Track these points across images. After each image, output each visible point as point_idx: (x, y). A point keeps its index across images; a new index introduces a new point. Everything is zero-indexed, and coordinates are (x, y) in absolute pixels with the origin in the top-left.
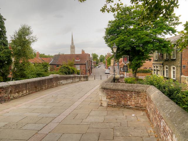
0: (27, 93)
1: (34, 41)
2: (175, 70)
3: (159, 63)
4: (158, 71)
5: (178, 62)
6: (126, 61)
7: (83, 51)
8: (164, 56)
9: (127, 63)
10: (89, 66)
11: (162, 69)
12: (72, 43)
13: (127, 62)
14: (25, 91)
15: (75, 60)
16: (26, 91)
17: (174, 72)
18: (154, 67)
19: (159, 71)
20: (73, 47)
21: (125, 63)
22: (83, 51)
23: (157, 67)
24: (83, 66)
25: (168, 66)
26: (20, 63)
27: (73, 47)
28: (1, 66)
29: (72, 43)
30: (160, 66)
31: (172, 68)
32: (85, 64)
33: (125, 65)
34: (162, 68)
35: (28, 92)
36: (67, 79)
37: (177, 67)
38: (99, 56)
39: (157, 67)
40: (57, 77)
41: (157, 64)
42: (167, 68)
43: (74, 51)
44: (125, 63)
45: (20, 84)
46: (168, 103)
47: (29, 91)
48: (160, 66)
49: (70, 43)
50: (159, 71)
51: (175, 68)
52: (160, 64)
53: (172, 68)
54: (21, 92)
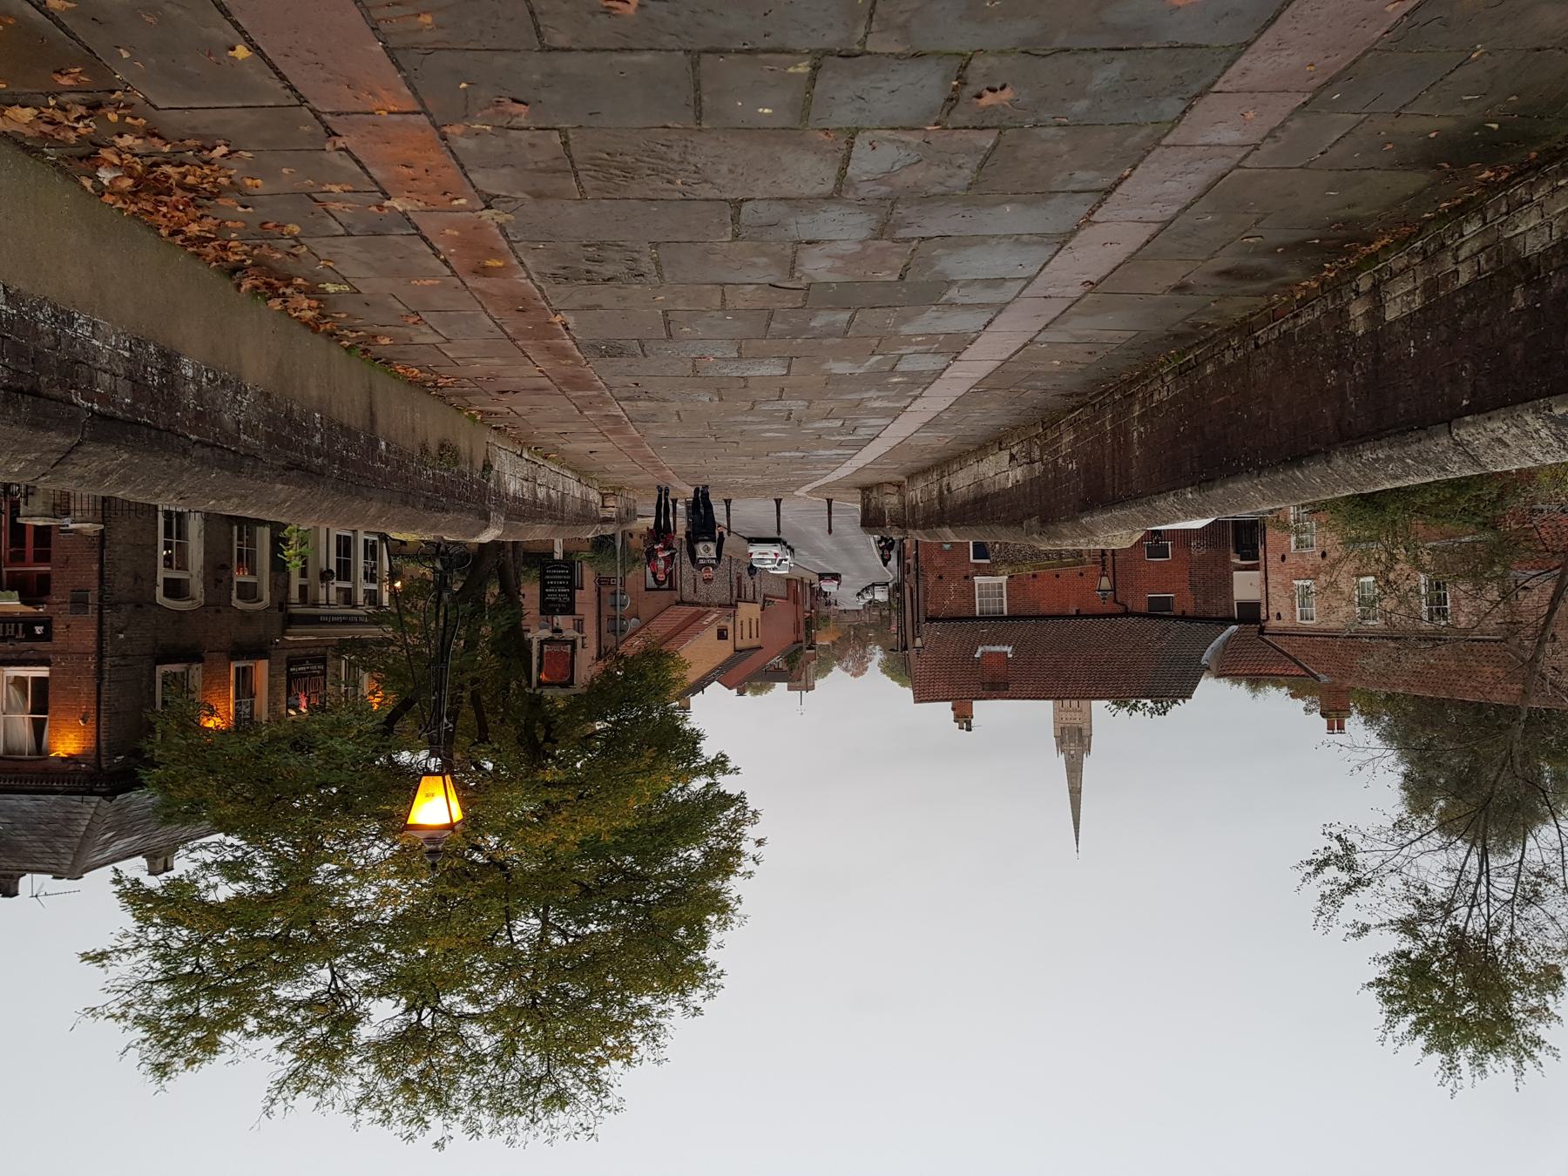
0: (1365, 283)
1: (1399, 824)
2: (162, 573)
3: (325, 630)
5: (128, 639)
6: (555, 648)
7: (964, 718)
10: (908, 609)
11: (296, 582)
12: (1074, 771)
14: (1391, 314)
15: (1015, 652)
16: (1375, 314)
17: (178, 559)
20: (1074, 741)
22: (964, 718)
25: (237, 603)
27: (1074, 741)
29: (1074, 771)
30: (316, 605)
31: (197, 587)
34: (295, 594)
35: (1358, 309)
36: (975, 501)
37: (143, 603)
39: (348, 597)
41: (347, 621)
42: (248, 592)
45: (1483, 407)
47: (1343, 313)
48: (316, 605)
49: (1091, 765)
50: (325, 576)
51: (160, 591)
52: (314, 620)
53: (197, 587)
54: (1464, 278)
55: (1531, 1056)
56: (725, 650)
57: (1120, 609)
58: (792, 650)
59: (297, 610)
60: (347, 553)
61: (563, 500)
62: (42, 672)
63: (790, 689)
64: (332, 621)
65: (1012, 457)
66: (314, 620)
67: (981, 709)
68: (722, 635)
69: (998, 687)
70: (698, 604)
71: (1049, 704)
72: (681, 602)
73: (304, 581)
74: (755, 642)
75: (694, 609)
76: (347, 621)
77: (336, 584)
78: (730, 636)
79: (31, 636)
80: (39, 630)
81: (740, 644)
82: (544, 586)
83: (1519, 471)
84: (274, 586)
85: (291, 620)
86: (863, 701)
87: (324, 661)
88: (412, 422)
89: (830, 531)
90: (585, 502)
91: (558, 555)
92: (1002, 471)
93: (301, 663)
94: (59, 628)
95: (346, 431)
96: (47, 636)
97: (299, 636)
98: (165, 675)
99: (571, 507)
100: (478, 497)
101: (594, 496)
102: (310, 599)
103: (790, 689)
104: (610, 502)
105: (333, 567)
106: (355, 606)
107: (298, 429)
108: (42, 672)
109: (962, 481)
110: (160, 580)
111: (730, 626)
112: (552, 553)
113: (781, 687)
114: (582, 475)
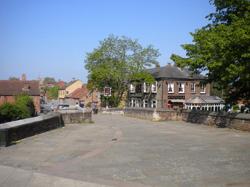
5: (159, 96)
52: (138, 98)
55: (31, 167)
56: (67, 89)
57: (6, 97)
59: (140, 99)
62: (180, 92)
66: (138, 98)
68: (67, 92)
78: (66, 92)
79: (170, 96)
80: (169, 97)
81: (64, 91)
83: (168, 133)
94: (167, 98)
96: (168, 96)
98: (204, 92)
108: (180, 92)
110: (156, 103)
111: (66, 94)
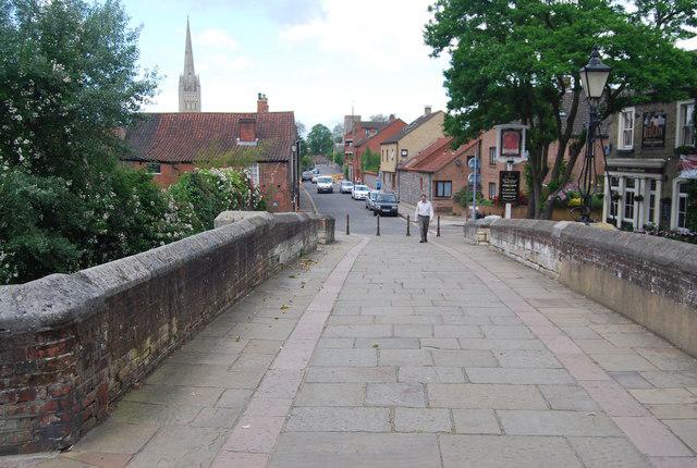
4: (630, 198)
7: (263, 102)
8: (674, 131)
9: (517, 160)
11: (658, 193)
12: (189, 64)
13: (519, 155)
18: (614, 182)
19: (640, 199)
21: (510, 159)
22: (263, 102)
23: (629, 183)
24: (275, 170)
26: (658, 28)
28: (4, 230)
29: (189, 64)
32: (284, 162)
33: (510, 168)
35: (175, 329)
38: (309, 130)
39: (629, 183)
40: (267, 226)
41: (629, 169)
43: (198, 103)
44: (510, 159)
46: (613, 328)
48: (647, 179)
49: (180, 70)
50: (640, 199)
52: (648, 170)
56: (403, 143)
58: (367, 142)
59: (658, 177)
60: (627, 208)
61: (514, 241)
63: (360, 117)
64: (638, 169)
65: (278, 260)
66: (648, 170)
67: (253, 108)
69: (245, 121)
70: (420, 172)
71: (203, 110)
72: (430, 173)
73: (653, 193)
74: (384, 148)
75: (424, 169)
76: (629, 169)
77: (636, 191)
81: (394, 146)
82: (517, 189)
84: (670, 190)
85: (660, 171)
86: (318, 107)
87: (643, 146)
88: (591, 278)
89: (408, 234)
90: (499, 238)
91: (508, 206)
92: (281, 251)
93: (657, 146)
95: (638, 283)
97: (656, 162)
99: (510, 237)
100: (566, 246)
101: (493, 241)
102: (649, 183)
103: (360, 117)
104: (482, 237)
105: (636, 203)
106: (624, 177)
107: (663, 285)
109: (298, 245)
112: (512, 206)
113: (366, 118)
114: (501, 254)
